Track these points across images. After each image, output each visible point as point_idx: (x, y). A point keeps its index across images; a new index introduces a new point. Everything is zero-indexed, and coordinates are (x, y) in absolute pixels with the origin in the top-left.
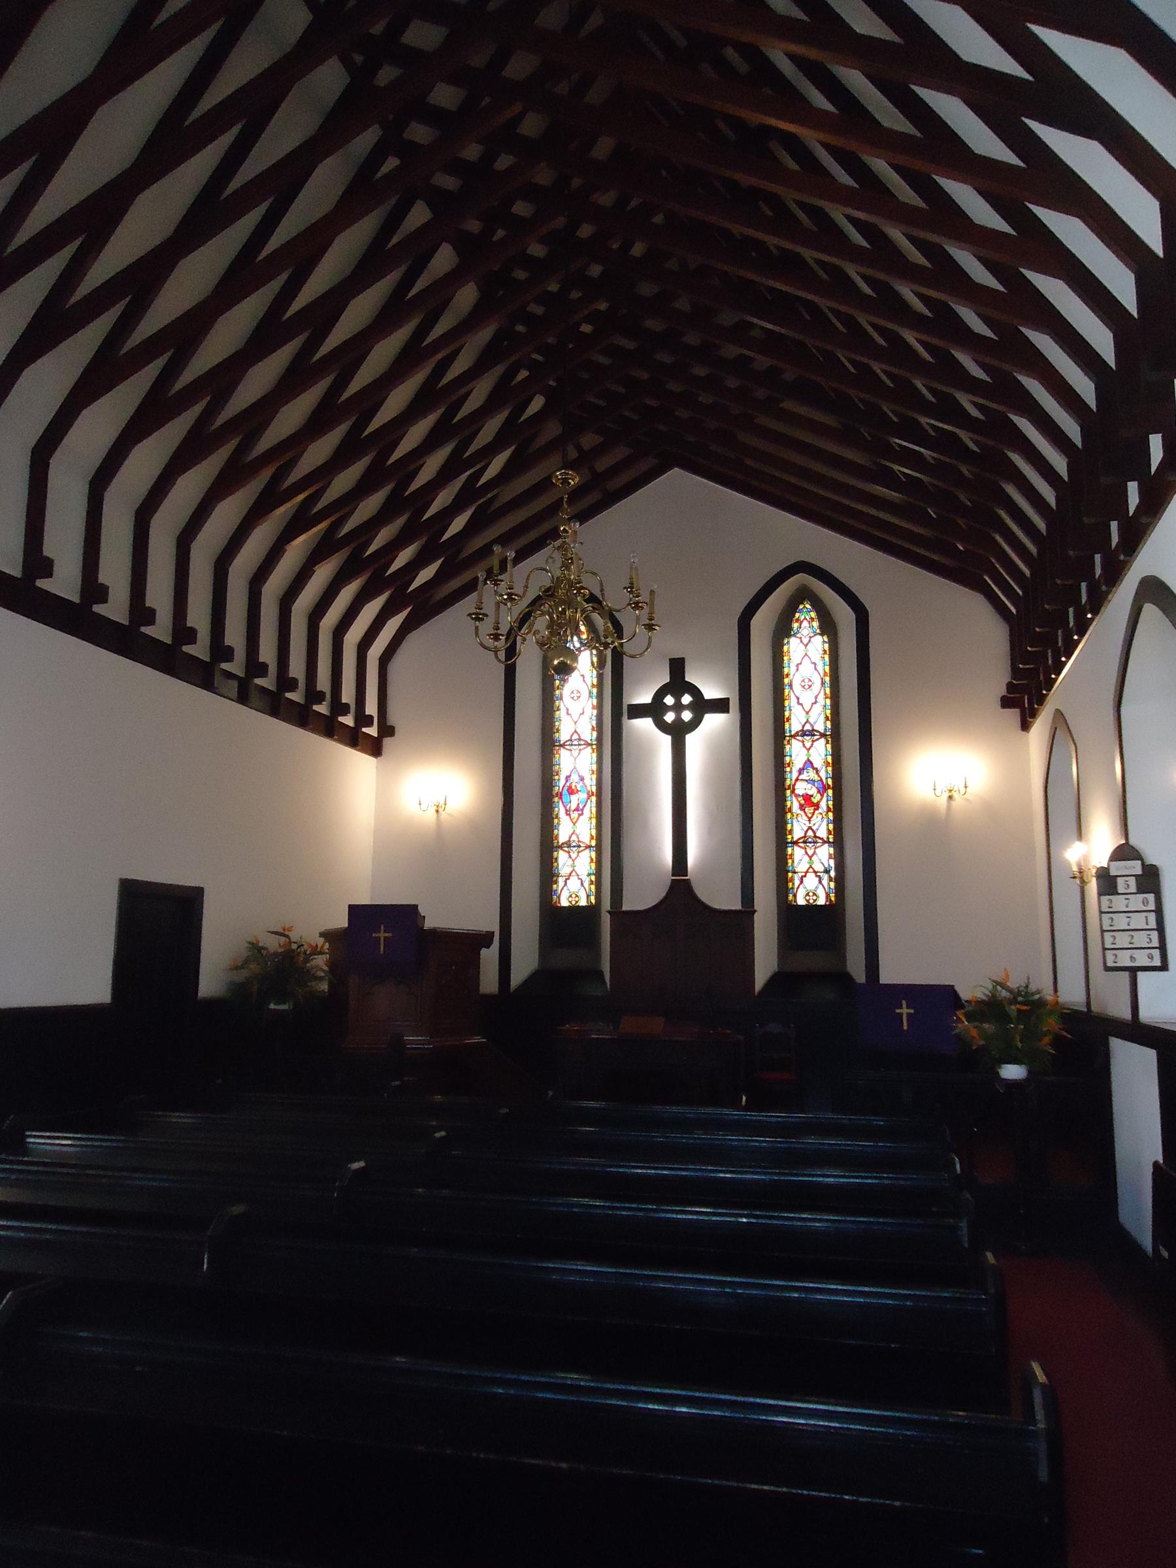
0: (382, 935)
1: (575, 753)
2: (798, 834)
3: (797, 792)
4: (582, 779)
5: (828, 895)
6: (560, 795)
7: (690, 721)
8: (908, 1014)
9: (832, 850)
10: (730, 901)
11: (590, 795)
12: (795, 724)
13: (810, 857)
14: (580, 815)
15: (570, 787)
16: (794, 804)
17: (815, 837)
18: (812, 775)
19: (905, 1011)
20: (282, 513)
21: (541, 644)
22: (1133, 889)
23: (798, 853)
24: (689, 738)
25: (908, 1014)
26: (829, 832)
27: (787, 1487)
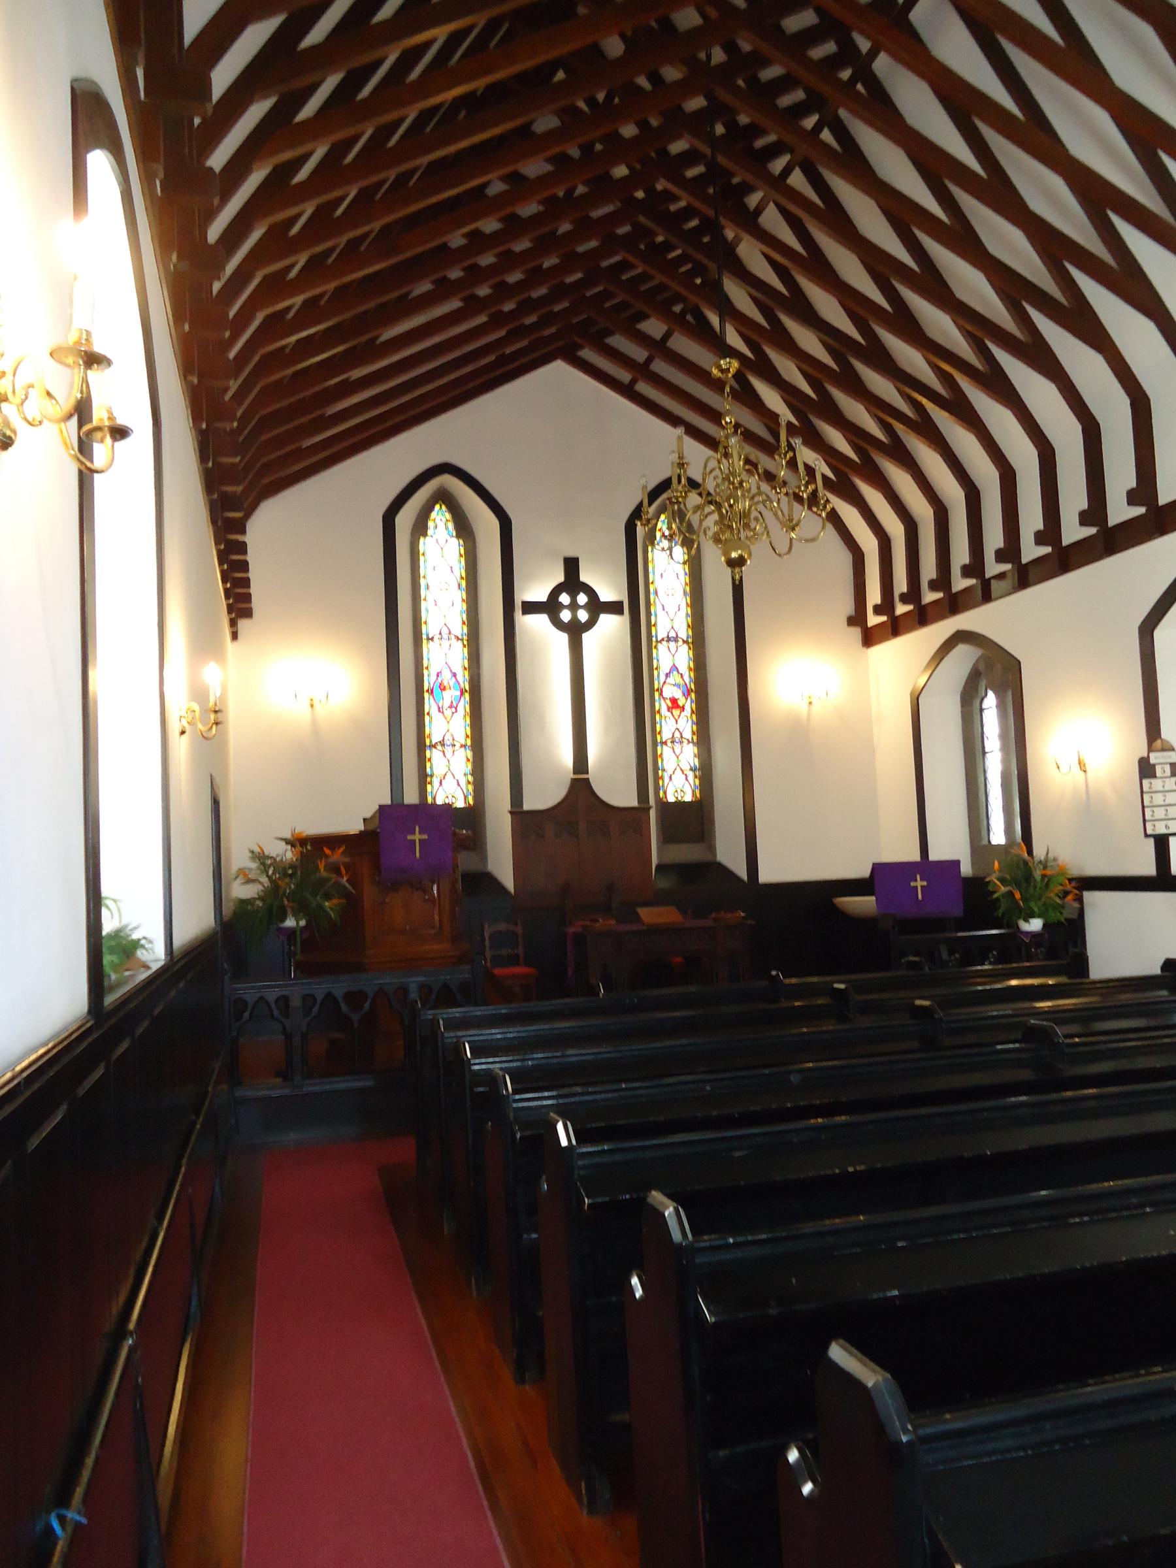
0: (417, 837)
2: (666, 735)
3: (665, 694)
4: (454, 675)
5: (693, 792)
6: (431, 692)
8: (922, 887)
9: (696, 750)
10: (629, 799)
18: (679, 680)
19: (919, 883)
20: (942, 419)
21: (717, 540)
22: (1168, 773)
24: (586, 637)
25: (922, 887)
26: (693, 733)
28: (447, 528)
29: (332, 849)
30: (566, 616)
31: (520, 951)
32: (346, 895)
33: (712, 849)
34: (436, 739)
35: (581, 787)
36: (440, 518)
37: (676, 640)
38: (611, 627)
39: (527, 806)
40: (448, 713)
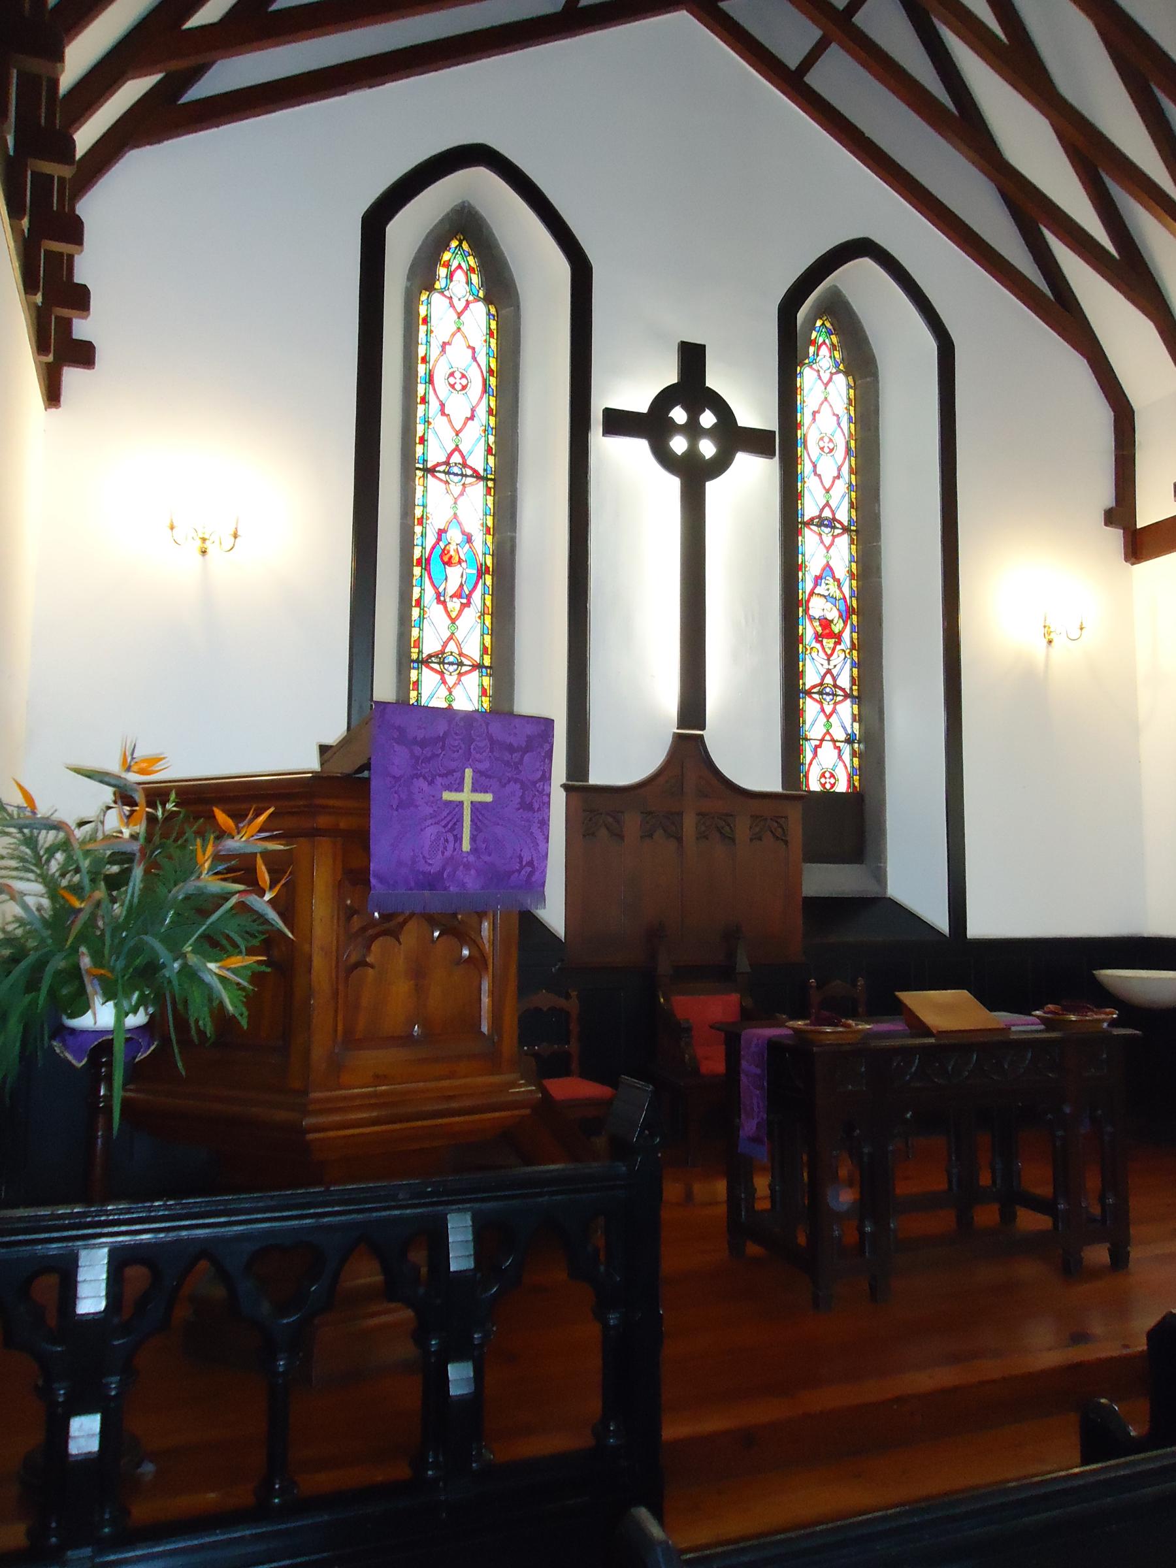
0: (467, 796)
1: (456, 489)
3: (811, 612)
4: (469, 539)
6: (425, 563)
7: (714, 459)
11: (481, 572)
12: (810, 508)
13: (828, 717)
14: (464, 606)
15: (444, 552)
16: (808, 631)
17: (835, 686)
18: (833, 590)
23: (810, 707)
24: (714, 489)
27: (289, 1558)
28: (469, 282)
29: (238, 817)
30: (679, 445)
31: (573, 1047)
32: (269, 942)
33: (880, 876)
34: (430, 646)
35: (689, 748)
36: (459, 277)
37: (831, 523)
38: (752, 473)
39: (597, 776)
40: (454, 605)
